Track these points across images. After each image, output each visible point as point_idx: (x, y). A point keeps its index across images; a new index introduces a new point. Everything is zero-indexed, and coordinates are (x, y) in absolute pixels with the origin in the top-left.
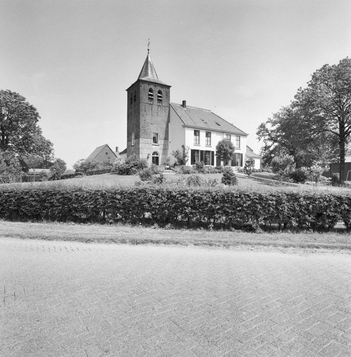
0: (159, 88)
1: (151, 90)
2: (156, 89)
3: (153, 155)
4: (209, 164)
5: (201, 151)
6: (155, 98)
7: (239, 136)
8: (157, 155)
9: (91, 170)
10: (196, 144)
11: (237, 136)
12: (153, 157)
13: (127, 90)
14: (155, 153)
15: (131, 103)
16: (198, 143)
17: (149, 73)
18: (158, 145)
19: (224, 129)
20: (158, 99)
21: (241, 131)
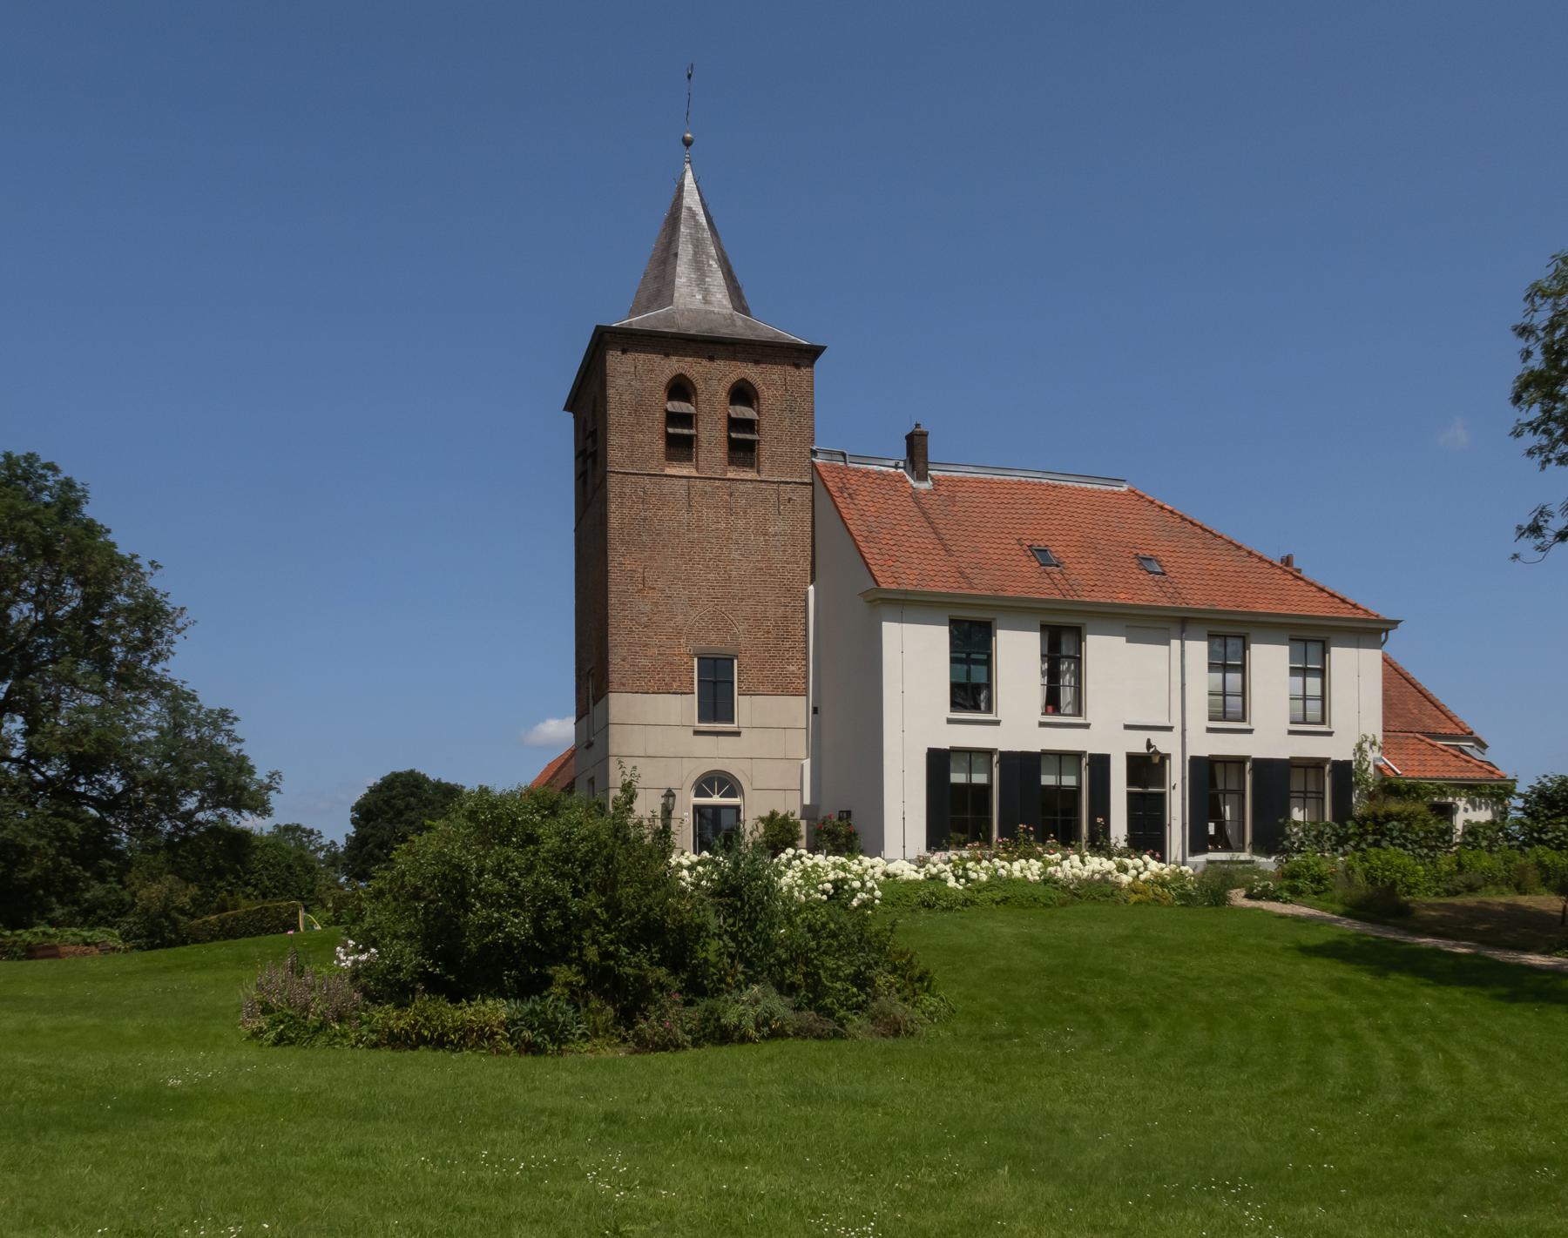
0: (726, 373)
1: (680, 388)
2: (714, 378)
3: (700, 792)
4: (1099, 843)
5: (1092, 756)
6: (711, 435)
7: (1322, 635)
8: (732, 793)
9: (499, 925)
10: (1305, 722)
11: (1306, 641)
12: (698, 809)
13: (568, 407)
14: (706, 783)
15: (585, 482)
16: (1314, 708)
17: (681, 281)
18: (737, 734)
19: (1197, 599)
20: (668, 436)
21: (1343, 601)
